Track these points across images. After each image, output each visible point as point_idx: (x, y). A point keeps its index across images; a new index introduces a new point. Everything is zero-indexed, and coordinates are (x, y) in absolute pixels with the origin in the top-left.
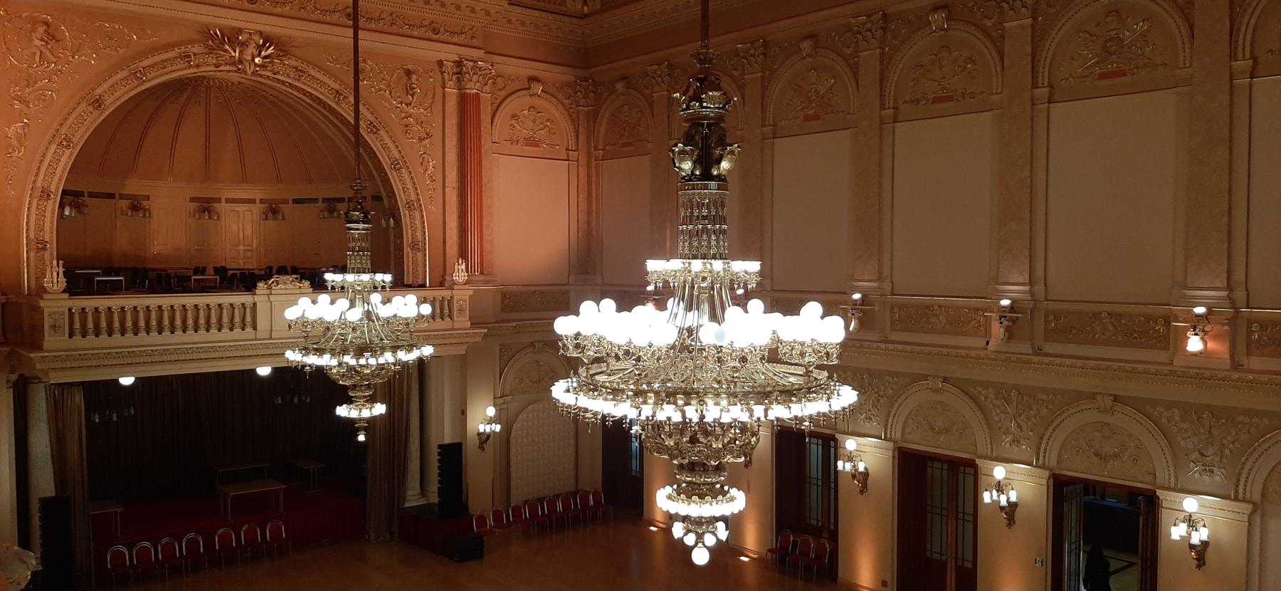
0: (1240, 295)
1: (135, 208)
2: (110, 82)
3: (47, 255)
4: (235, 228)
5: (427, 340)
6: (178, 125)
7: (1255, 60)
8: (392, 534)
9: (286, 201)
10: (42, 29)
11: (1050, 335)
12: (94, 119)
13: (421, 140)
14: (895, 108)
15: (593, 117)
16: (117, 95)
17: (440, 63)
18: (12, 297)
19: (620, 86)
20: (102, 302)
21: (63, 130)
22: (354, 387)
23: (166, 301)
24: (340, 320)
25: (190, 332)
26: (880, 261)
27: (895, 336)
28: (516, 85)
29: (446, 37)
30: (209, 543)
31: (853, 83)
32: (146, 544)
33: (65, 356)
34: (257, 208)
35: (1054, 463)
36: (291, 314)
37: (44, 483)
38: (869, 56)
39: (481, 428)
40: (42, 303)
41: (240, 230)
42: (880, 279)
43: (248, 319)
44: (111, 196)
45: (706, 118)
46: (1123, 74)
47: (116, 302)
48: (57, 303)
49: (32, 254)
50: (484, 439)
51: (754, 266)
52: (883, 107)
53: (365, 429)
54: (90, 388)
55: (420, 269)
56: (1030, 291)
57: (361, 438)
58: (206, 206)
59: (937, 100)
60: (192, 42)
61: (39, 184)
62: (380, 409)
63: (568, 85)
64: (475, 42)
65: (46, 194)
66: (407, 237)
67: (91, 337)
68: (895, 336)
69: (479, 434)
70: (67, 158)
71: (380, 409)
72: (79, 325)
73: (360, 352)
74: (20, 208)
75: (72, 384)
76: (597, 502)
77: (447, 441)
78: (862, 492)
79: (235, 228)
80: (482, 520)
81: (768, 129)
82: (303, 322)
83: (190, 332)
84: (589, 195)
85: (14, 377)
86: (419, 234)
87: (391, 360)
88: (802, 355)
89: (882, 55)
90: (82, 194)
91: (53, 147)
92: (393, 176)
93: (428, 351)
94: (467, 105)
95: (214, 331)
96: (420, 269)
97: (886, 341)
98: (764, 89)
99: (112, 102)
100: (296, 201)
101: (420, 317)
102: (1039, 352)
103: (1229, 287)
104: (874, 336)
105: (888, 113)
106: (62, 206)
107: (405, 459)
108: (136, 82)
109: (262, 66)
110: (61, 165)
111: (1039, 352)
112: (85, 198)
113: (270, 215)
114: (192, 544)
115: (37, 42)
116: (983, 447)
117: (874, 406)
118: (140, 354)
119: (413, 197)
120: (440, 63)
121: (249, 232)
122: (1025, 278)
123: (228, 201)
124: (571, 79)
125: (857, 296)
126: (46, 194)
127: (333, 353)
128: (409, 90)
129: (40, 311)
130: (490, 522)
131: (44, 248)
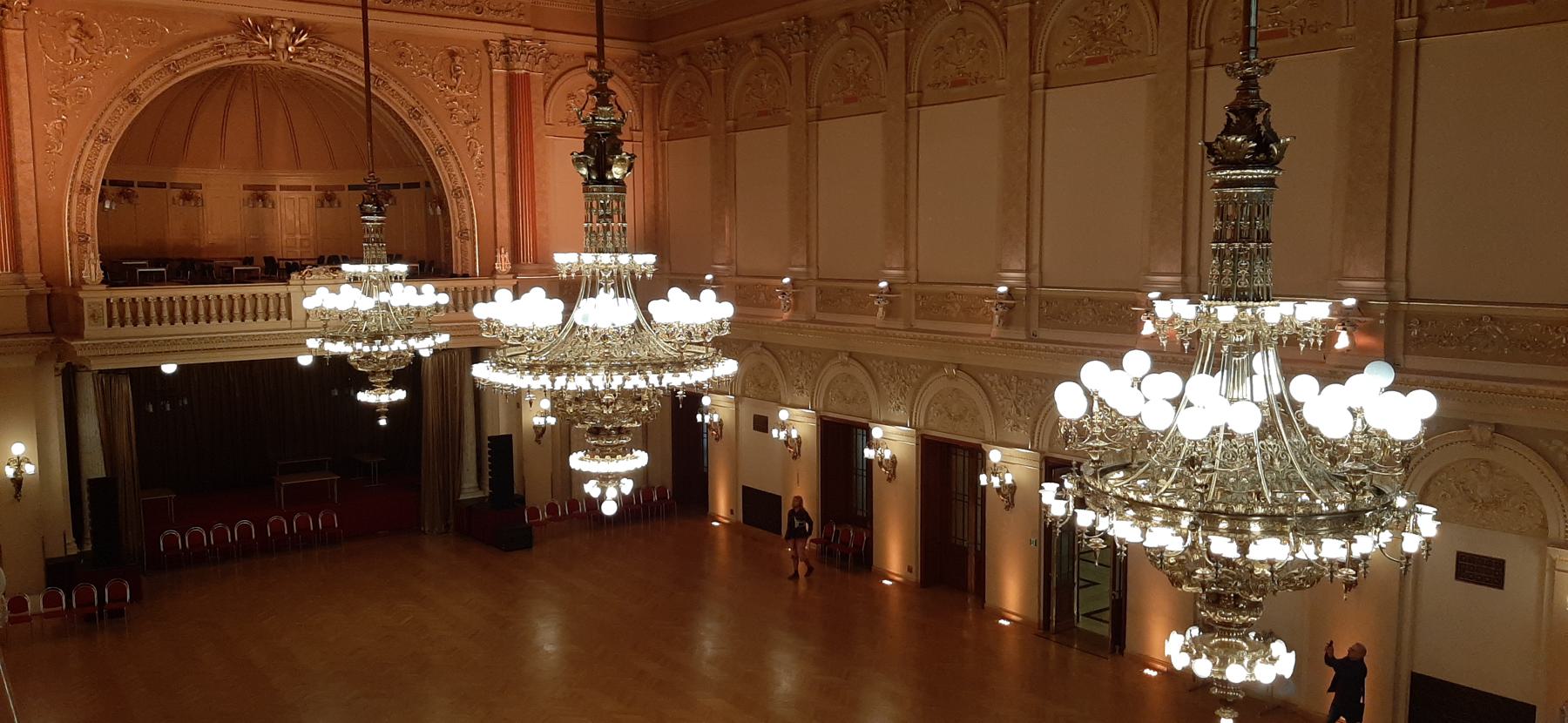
0: (1399, 286)
1: (187, 197)
2: (145, 76)
3: (89, 247)
4: (291, 217)
5: (443, 331)
6: (228, 105)
7: (1209, 47)
8: (447, 526)
9: (342, 188)
10: (75, 27)
11: (1043, 321)
12: (129, 114)
13: (467, 124)
14: (920, 91)
15: (658, 93)
16: (152, 88)
17: (486, 43)
18: (58, 290)
19: (680, 61)
20: (139, 293)
21: (100, 126)
22: (374, 373)
23: (212, 291)
24: (357, 307)
25: (226, 321)
26: (906, 249)
27: (920, 324)
28: (571, 62)
29: (491, 16)
30: (261, 530)
31: (1152, 15)
32: (199, 529)
33: (104, 343)
34: (312, 196)
35: (1045, 447)
36: (309, 303)
37: (94, 466)
38: (896, 36)
39: (538, 421)
40: (81, 294)
41: (293, 217)
42: (906, 267)
43: (283, 309)
44: (162, 185)
45: (602, 129)
46: (1104, 60)
47: (152, 293)
48: (96, 295)
49: (75, 247)
50: (540, 431)
51: (650, 259)
52: (908, 91)
53: (386, 414)
54: (133, 373)
55: (469, 257)
56: (1182, 282)
57: (383, 422)
58: (260, 194)
59: (956, 84)
60: (225, 33)
61: (79, 177)
62: (400, 395)
63: (631, 60)
64: (523, 20)
65: (85, 189)
66: (455, 226)
67: (129, 326)
68: (920, 324)
69: (535, 427)
70: (106, 152)
71: (400, 395)
72: (117, 315)
73: (373, 337)
74: (61, 205)
75: (117, 372)
76: (662, 497)
77: (503, 432)
78: (889, 480)
79: (291, 217)
80: (534, 513)
81: (812, 111)
82: (321, 312)
83: (226, 321)
84: (656, 179)
85: (61, 365)
86: (467, 221)
87: (404, 347)
88: (705, 334)
89: (906, 36)
90: (131, 184)
91: (92, 142)
92: (437, 162)
93: (443, 339)
94: (517, 88)
95: (249, 321)
96: (469, 257)
97: (813, 321)
98: (808, 68)
99: (147, 96)
100: (351, 188)
101: (437, 307)
102: (1032, 337)
103: (1388, 277)
104: (899, 324)
105: (913, 96)
106: (102, 199)
107: (461, 448)
108: (170, 76)
109: (297, 54)
110: (100, 158)
111: (1032, 337)
112: (136, 188)
113: (326, 203)
114: (245, 531)
115: (72, 40)
116: (989, 432)
117: (902, 394)
118: (175, 343)
119: (460, 184)
120: (486, 43)
121: (305, 219)
122: (1022, 266)
123: (283, 188)
124: (636, 54)
125: (883, 284)
126: (85, 189)
127: (348, 341)
128: (454, 73)
129: (79, 301)
130: (543, 515)
131: (86, 241)
